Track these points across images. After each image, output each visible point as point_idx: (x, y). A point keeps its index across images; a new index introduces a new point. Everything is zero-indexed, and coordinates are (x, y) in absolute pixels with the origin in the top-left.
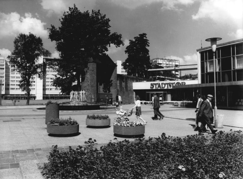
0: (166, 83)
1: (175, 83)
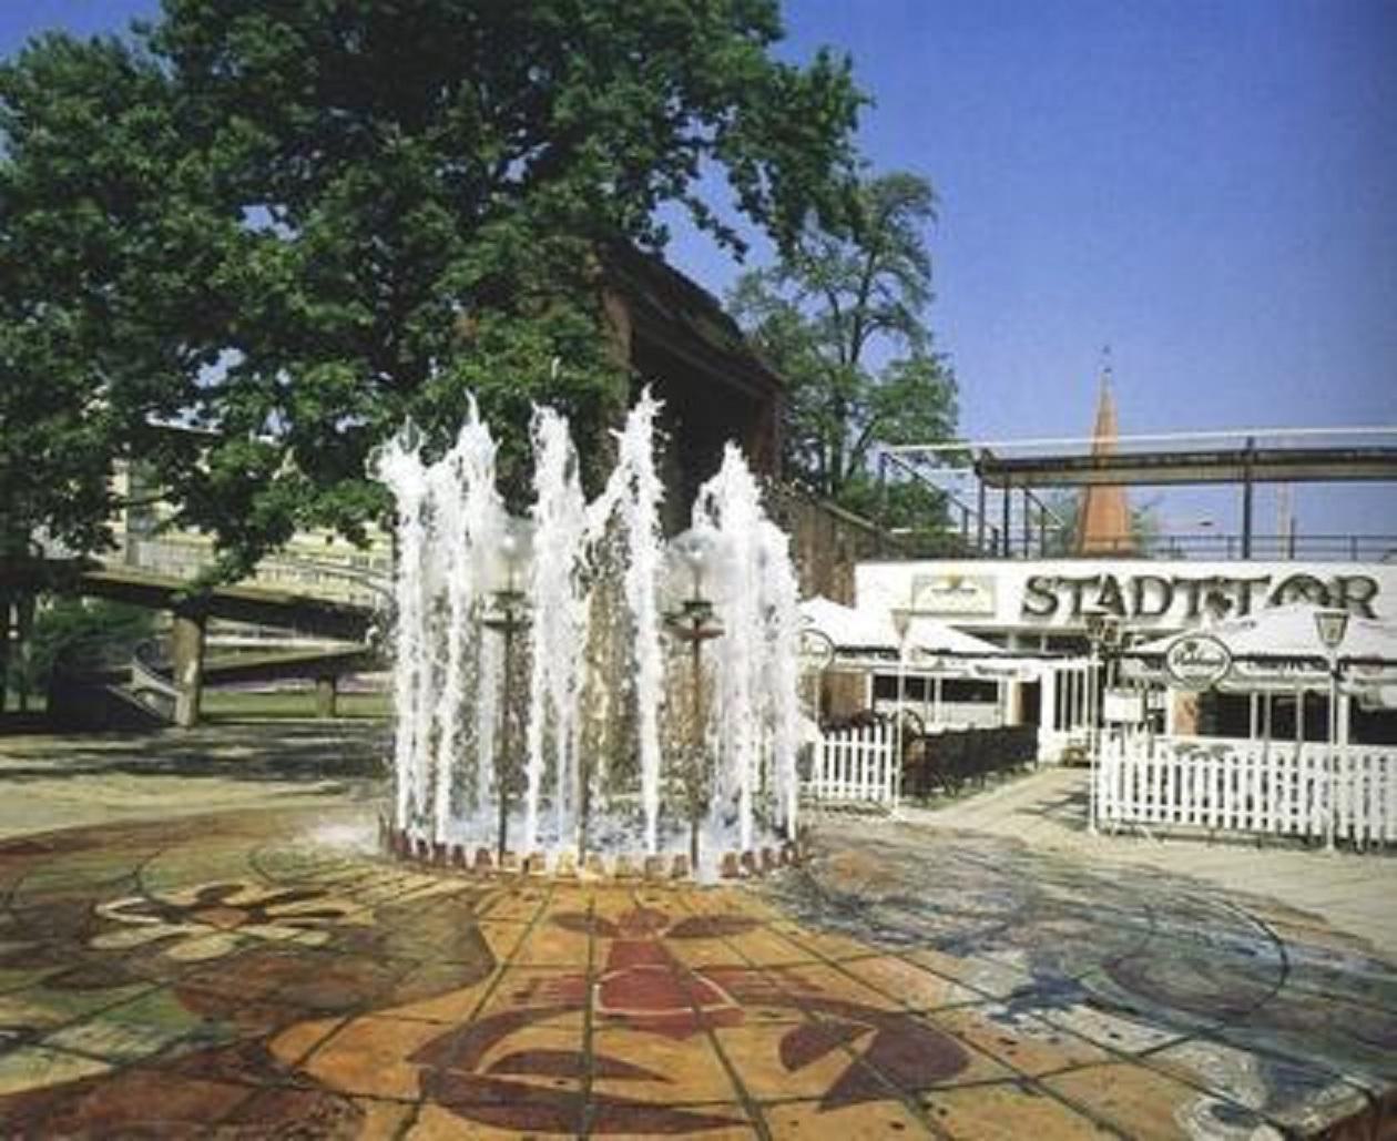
0: (1177, 581)
1: (1266, 580)
